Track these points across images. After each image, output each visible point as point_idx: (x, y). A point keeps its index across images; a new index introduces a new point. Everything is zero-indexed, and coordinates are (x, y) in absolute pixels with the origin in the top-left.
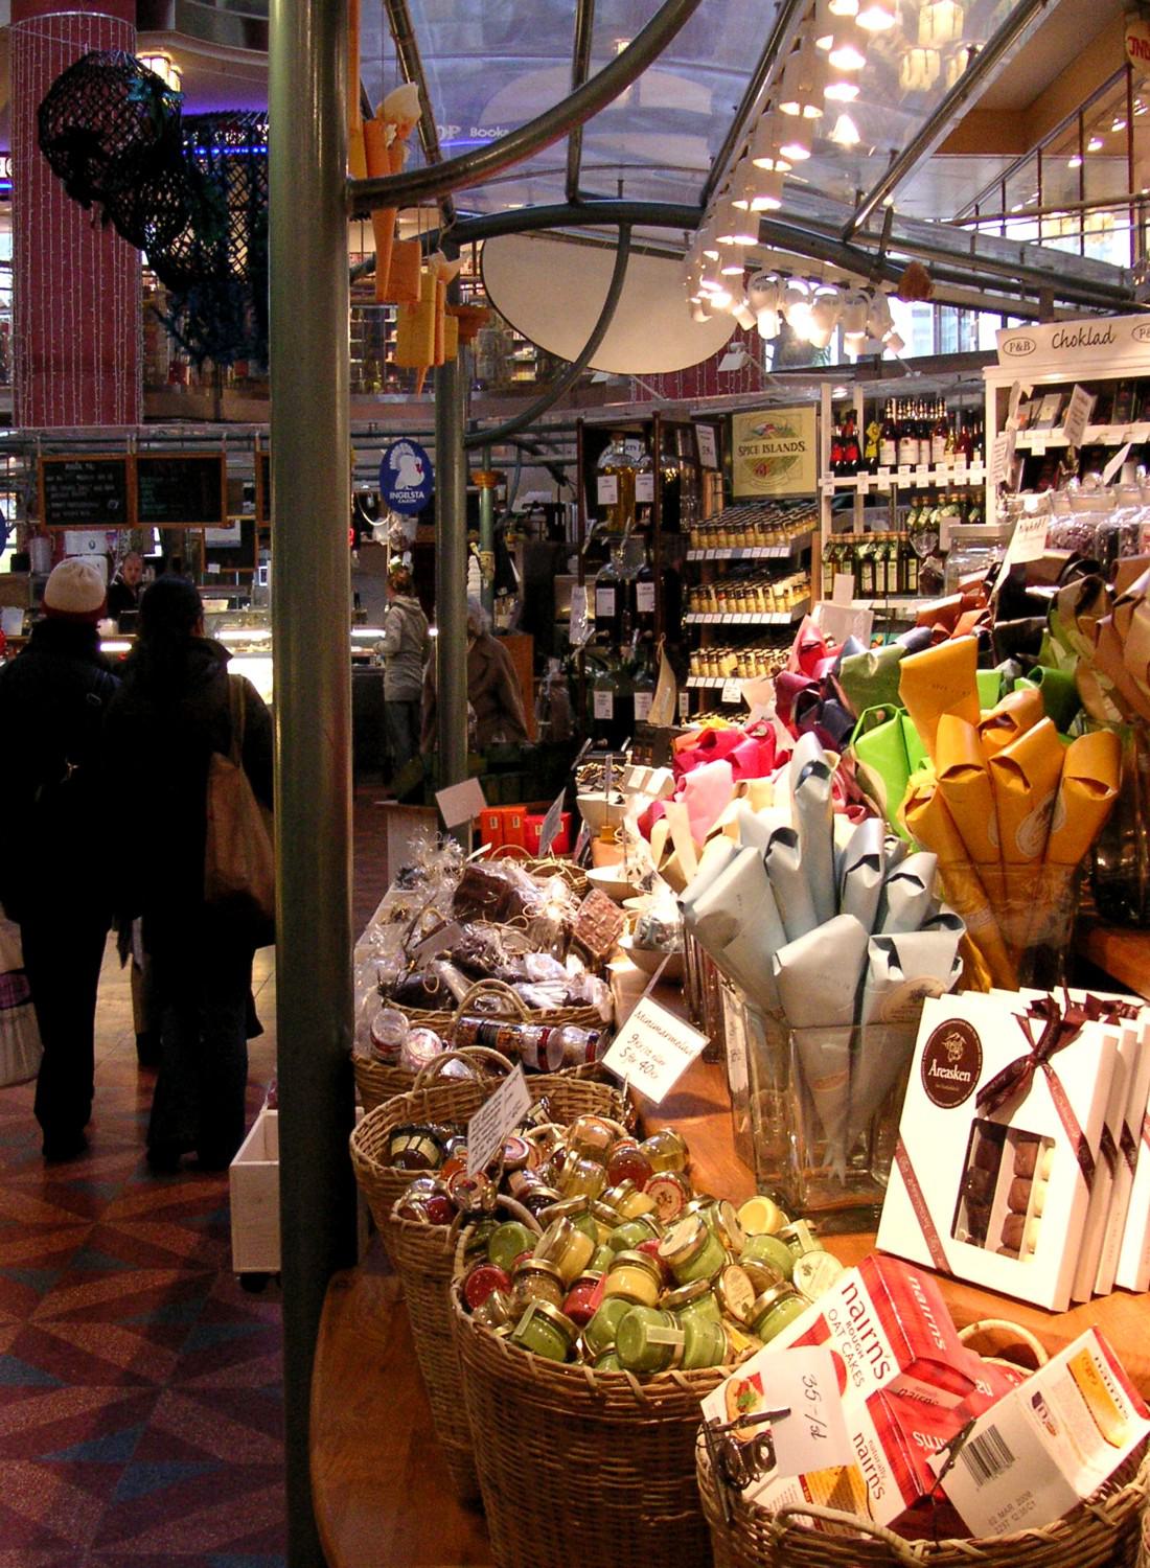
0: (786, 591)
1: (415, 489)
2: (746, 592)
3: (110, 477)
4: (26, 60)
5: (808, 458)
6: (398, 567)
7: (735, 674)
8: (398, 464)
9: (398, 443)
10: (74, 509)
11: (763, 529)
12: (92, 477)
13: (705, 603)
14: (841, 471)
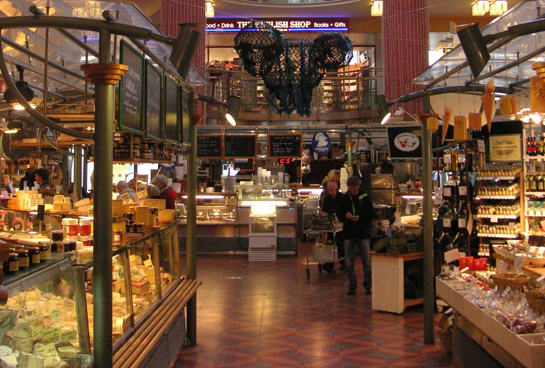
0: (513, 189)
1: (324, 147)
2: (498, 190)
3: (215, 142)
4: (168, 3)
5: (518, 151)
6: (305, 170)
7: (494, 213)
8: (318, 139)
9: (318, 132)
10: (201, 152)
11: (504, 171)
12: (209, 142)
13: (483, 192)
14: (531, 155)
